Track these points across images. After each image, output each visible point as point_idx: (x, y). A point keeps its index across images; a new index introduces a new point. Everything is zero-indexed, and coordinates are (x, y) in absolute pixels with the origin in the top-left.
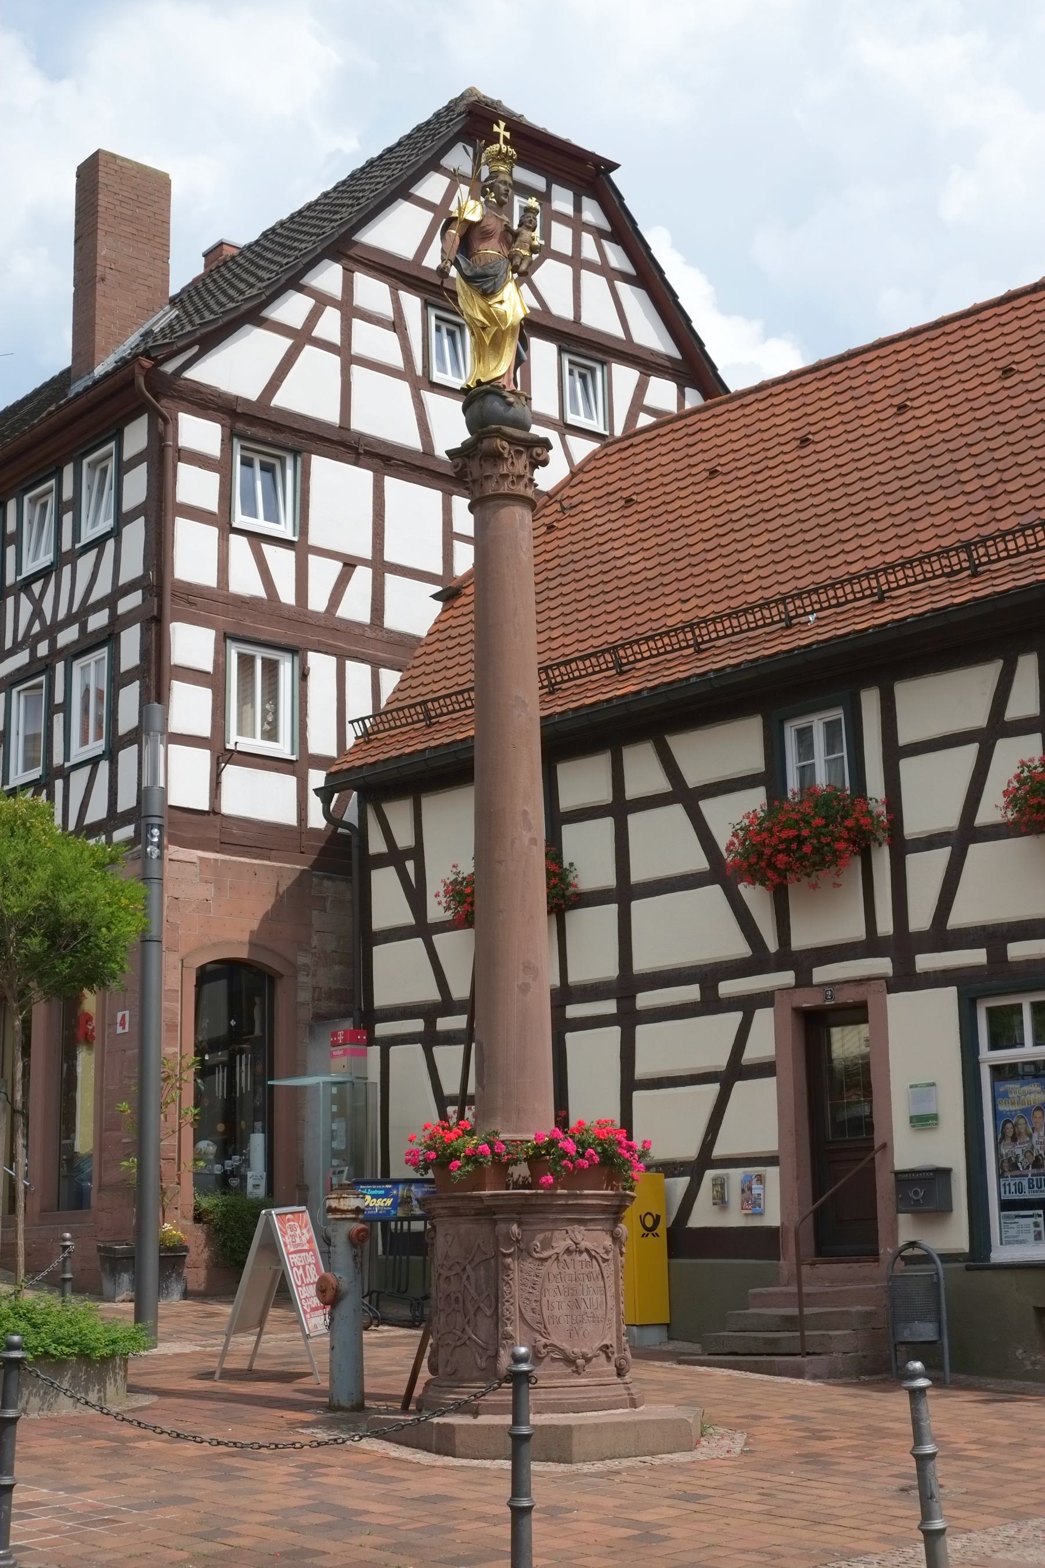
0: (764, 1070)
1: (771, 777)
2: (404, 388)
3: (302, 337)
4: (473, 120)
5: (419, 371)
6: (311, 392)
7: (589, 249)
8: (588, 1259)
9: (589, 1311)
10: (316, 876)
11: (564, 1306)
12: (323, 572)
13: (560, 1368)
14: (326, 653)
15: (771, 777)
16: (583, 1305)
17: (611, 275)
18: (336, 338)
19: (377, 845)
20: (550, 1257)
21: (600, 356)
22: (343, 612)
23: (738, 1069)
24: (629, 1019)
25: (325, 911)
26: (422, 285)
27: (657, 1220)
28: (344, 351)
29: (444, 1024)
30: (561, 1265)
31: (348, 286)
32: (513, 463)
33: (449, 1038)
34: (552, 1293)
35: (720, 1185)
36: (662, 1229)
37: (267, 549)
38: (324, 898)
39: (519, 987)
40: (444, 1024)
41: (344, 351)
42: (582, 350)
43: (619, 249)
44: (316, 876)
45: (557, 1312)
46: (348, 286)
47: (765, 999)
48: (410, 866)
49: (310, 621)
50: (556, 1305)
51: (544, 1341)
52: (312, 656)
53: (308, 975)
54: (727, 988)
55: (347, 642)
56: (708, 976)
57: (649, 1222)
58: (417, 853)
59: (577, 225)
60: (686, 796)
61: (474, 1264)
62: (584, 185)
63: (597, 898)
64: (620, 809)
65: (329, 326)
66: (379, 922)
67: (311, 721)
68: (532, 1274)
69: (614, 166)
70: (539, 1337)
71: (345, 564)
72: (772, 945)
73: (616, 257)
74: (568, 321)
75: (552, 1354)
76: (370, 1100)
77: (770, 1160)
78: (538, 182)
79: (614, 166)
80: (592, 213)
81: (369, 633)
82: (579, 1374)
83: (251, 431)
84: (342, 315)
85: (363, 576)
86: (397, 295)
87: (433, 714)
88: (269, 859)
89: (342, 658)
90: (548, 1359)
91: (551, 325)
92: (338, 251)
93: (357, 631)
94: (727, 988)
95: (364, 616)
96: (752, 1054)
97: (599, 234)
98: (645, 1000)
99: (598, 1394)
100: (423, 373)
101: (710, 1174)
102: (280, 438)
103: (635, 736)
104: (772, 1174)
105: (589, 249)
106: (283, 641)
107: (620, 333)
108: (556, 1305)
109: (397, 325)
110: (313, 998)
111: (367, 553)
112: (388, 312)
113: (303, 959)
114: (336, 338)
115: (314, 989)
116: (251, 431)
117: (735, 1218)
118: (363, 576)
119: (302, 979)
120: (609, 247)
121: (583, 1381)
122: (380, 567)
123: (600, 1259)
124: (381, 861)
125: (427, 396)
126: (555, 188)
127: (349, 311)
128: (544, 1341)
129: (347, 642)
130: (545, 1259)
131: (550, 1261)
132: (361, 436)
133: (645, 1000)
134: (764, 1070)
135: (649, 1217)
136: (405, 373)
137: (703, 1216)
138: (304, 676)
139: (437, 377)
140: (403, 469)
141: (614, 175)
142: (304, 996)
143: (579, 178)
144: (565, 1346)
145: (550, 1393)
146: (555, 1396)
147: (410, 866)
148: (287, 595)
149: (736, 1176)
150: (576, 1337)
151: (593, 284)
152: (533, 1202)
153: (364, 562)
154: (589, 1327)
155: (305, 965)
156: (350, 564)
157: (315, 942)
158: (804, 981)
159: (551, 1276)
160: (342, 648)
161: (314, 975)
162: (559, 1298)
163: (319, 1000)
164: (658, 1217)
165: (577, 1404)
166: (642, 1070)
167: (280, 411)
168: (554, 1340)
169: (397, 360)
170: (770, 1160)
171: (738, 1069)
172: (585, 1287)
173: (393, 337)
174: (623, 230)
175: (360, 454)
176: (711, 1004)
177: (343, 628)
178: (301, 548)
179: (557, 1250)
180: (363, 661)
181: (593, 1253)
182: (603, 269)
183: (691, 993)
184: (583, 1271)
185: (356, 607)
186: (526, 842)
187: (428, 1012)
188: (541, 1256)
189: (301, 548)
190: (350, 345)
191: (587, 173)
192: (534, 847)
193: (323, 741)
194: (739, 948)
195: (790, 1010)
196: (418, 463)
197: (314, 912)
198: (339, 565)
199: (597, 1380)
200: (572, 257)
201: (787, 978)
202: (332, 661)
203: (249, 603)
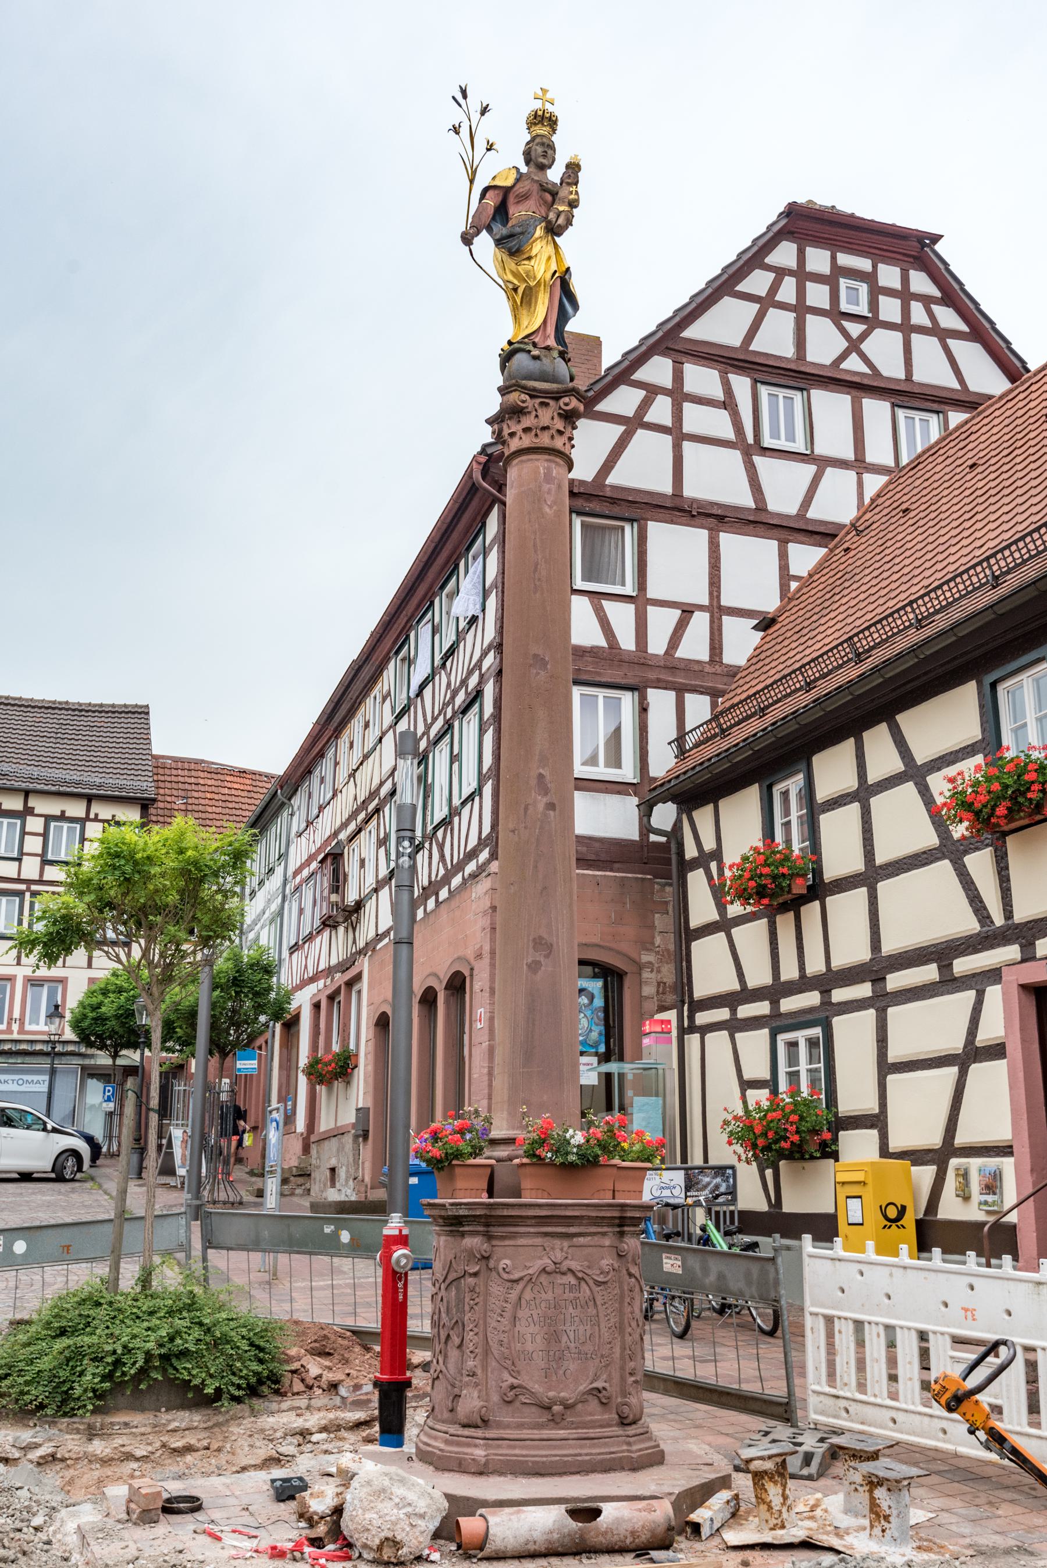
0: (997, 1051)
1: (991, 740)
2: (735, 457)
3: (634, 423)
4: (804, 223)
5: (750, 440)
6: (645, 467)
7: (918, 315)
8: (573, 1281)
9: (572, 1345)
10: (658, 883)
11: (539, 1339)
12: (661, 624)
13: (533, 1415)
14: (665, 689)
15: (991, 740)
16: (564, 1339)
17: (943, 335)
18: (668, 422)
19: (691, 852)
20: (521, 1279)
21: (935, 406)
22: (683, 652)
23: (973, 1053)
24: (882, 1002)
25: (668, 913)
26: (746, 365)
27: (902, 1211)
28: (677, 434)
29: (746, 1011)
30: (536, 1288)
31: (678, 377)
32: (537, 416)
33: (753, 1023)
34: (523, 1322)
35: (964, 1175)
36: (909, 1221)
37: (606, 604)
38: (666, 903)
39: (529, 966)
40: (746, 1011)
41: (677, 434)
42: (917, 404)
43: (950, 311)
44: (658, 883)
45: (529, 1347)
46: (678, 377)
47: (994, 975)
48: (713, 866)
49: (650, 663)
50: (528, 1337)
51: (511, 1380)
52: (652, 694)
53: (652, 971)
54: (962, 965)
55: (680, 676)
56: (942, 954)
57: (892, 1213)
58: (717, 855)
59: (905, 295)
60: (915, 773)
61: (448, 1282)
62: (911, 260)
63: (844, 884)
64: (864, 793)
65: (661, 411)
66: (696, 921)
67: (651, 748)
68: (502, 1298)
69: (936, 238)
70: (506, 1375)
71: (683, 611)
72: (999, 920)
73: (949, 319)
74: (898, 381)
75: (523, 1399)
76: (668, 1085)
77: (1005, 1150)
78: (864, 264)
79: (936, 238)
80: (921, 283)
81: (708, 669)
82: (557, 1423)
83: (589, 506)
84: (673, 400)
85: (700, 622)
86: (728, 381)
87: (725, 726)
88: (611, 870)
89: (681, 691)
90: (517, 1404)
91: (883, 385)
92: (667, 348)
93: (696, 668)
94: (962, 965)
95: (702, 654)
96: (986, 1035)
97: (927, 301)
98: (895, 981)
99: (578, 1451)
100: (755, 441)
101: (954, 1162)
102: (616, 510)
103: (869, 721)
104: (1007, 1164)
105: (918, 315)
106: (623, 681)
107: (957, 386)
108: (528, 1337)
109: (728, 404)
110: (658, 992)
111: (703, 598)
112: (719, 394)
113: (646, 958)
114: (668, 422)
115: (659, 984)
116: (589, 506)
117: (973, 1213)
118: (700, 622)
119: (646, 975)
120: (938, 310)
121: (562, 1433)
122: (717, 611)
123: (591, 1282)
124: (694, 864)
125: (757, 460)
126: (881, 267)
127: (679, 395)
128: (511, 1380)
129: (680, 676)
130: (516, 1281)
131: (521, 1284)
132: (694, 501)
133: (895, 981)
134: (997, 1051)
135: (891, 1208)
136: (738, 443)
137: (951, 1209)
138: (644, 710)
139: (767, 442)
140: (737, 525)
141: (938, 247)
142: (648, 990)
143: (905, 255)
144: (537, 1388)
145: (514, 1447)
146: (517, 1452)
147: (713, 866)
148: (627, 642)
149: (975, 1164)
150: (554, 1378)
151: (925, 347)
152: (499, 1212)
153: (701, 608)
154: (572, 1366)
155: (650, 963)
156: (687, 611)
157: (658, 941)
158: (1028, 956)
159: (523, 1301)
160: (681, 683)
161: (659, 971)
162: (532, 1329)
163: (664, 993)
164: (904, 1208)
165: (543, 1463)
166: (894, 1054)
167: (614, 488)
168: (524, 1380)
169: (728, 433)
170: (1005, 1150)
171: (973, 1053)
172: (568, 1317)
173: (724, 415)
174: (952, 293)
175: (693, 516)
176: (948, 983)
177: (682, 666)
178: (640, 601)
179: (530, 1271)
180: (702, 693)
181: (580, 1275)
182: (936, 331)
183: (930, 973)
184: (565, 1296)
185: (695, 646)
186: (541, 807)
187: (730, 1000)
188: (512, 1277)
189: (640, 601)
190: (681, 425)
191: (915, 249)
192: (552, 813)
193: (663, 762)
194: (969, 924)
195: (1016, 986)
196: (751, 518)
197: (657, 915)
198: (678, 612)
199: (582, 1432)
200: (902, 324)
201: (1012, 952)
202: (671, 695)
203: (593, 652)
